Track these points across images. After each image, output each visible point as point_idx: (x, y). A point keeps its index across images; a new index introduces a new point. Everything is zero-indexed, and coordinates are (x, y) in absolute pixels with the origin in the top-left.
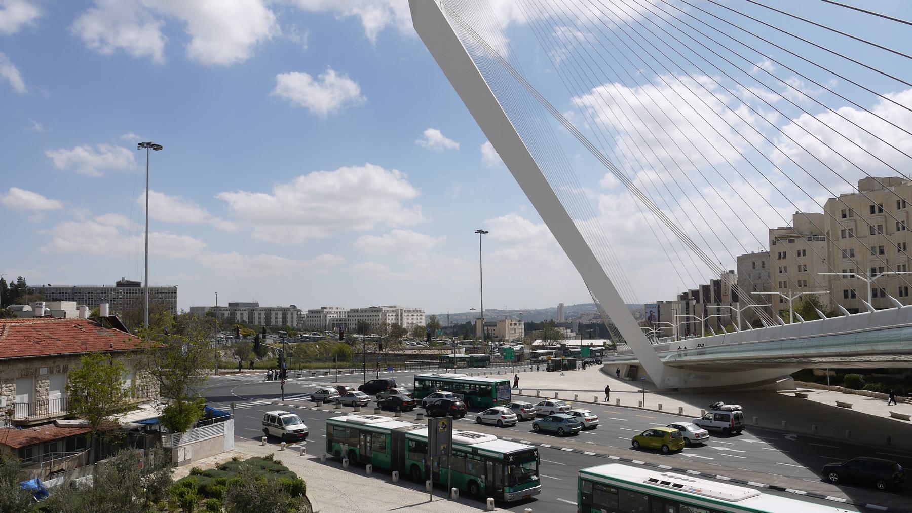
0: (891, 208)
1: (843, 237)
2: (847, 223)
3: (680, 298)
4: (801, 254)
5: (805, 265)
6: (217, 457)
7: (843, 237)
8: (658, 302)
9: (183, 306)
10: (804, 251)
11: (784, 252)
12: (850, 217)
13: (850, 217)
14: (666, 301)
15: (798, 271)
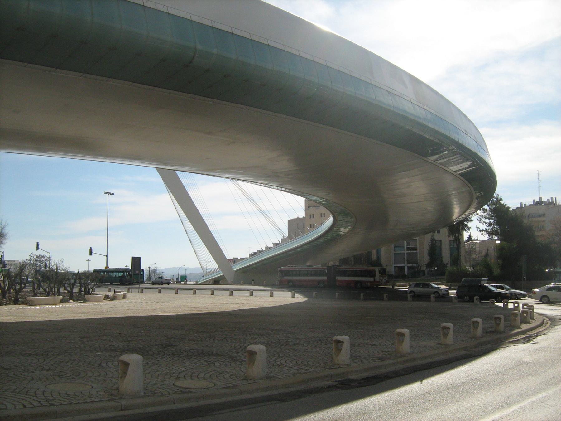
4: (323, 216)
10: (313, 215)
11: (313, 215)
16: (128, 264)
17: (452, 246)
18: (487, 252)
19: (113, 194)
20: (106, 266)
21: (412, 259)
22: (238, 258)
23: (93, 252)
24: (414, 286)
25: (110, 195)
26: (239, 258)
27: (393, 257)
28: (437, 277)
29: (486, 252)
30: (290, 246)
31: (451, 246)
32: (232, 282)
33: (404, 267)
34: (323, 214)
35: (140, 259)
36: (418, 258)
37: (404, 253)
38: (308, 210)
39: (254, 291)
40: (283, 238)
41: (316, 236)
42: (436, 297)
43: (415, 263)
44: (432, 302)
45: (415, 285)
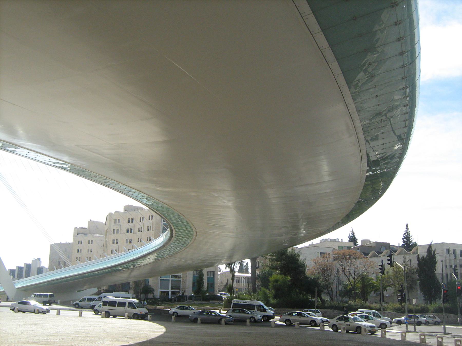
2: (116, 227)
6: (154, 308)
7: (114, 233)
10: (82, 242)
11: (81, 241)
12: (118, 223)
13: (118, 223)
15: (87, 252)
17: (209, 276)
21: (176, 286)
24: (232, 312)
27: (159, 282)
28: (203, 302)
31: (208, 276)
32: (13, 299)
33: (168, 292)
35: (92, 241)
36: (181, 285)
39: (61, 310)
41: (145, 253)
42: (251, 322)
44: (273, 327)
45: (232, 311)
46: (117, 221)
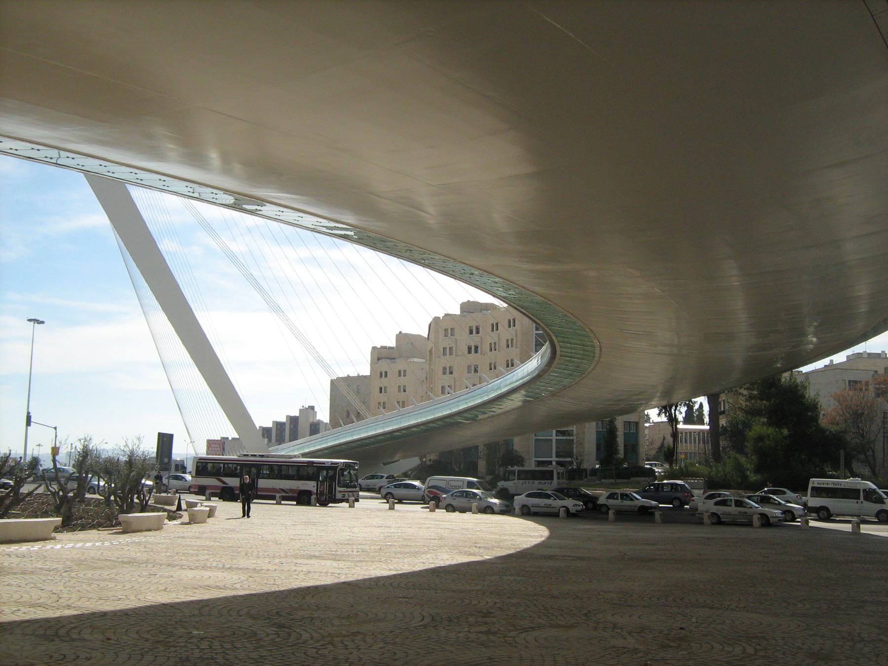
0: (486, 329)
1: (444, 354)
3: (275, 424)
4: (402, 374)
5: (405, 386)
7: (444, 354)
8: (223, 438)
9: (803, 372)
10: (386, 373)
12: (451, 336)
14: (232, 438)
16: (150, 447)
18: (663, 442)
19: (43, 322)
20: (54, 446)
21: (565, 450)
22: (228, 438)
23: (32, 420)
25: (36, 325)
26: (230, 439)
29: (662, 441)
30: (400, 423)
34: (402, 371)
35: (171, 437)
36: (575, 450)
37: (551, 440)
38: (377, 363)
40: (302, 408)
43: (568, 457)
46: (449, 332)
